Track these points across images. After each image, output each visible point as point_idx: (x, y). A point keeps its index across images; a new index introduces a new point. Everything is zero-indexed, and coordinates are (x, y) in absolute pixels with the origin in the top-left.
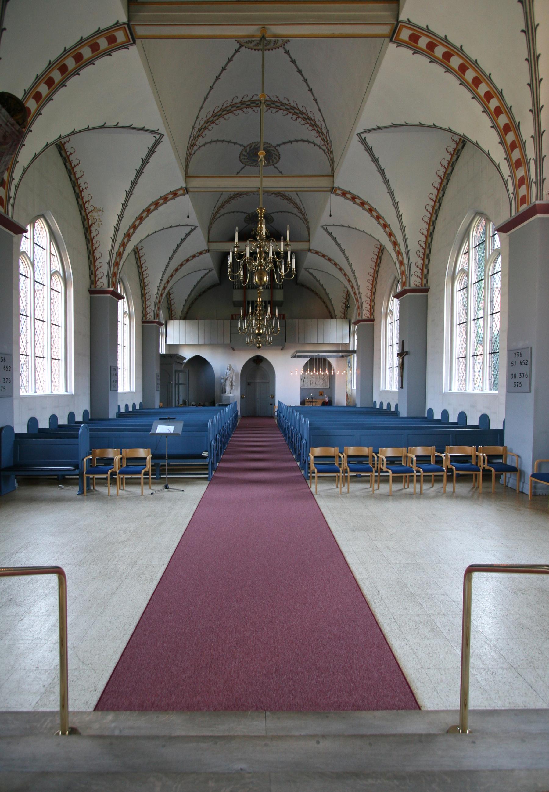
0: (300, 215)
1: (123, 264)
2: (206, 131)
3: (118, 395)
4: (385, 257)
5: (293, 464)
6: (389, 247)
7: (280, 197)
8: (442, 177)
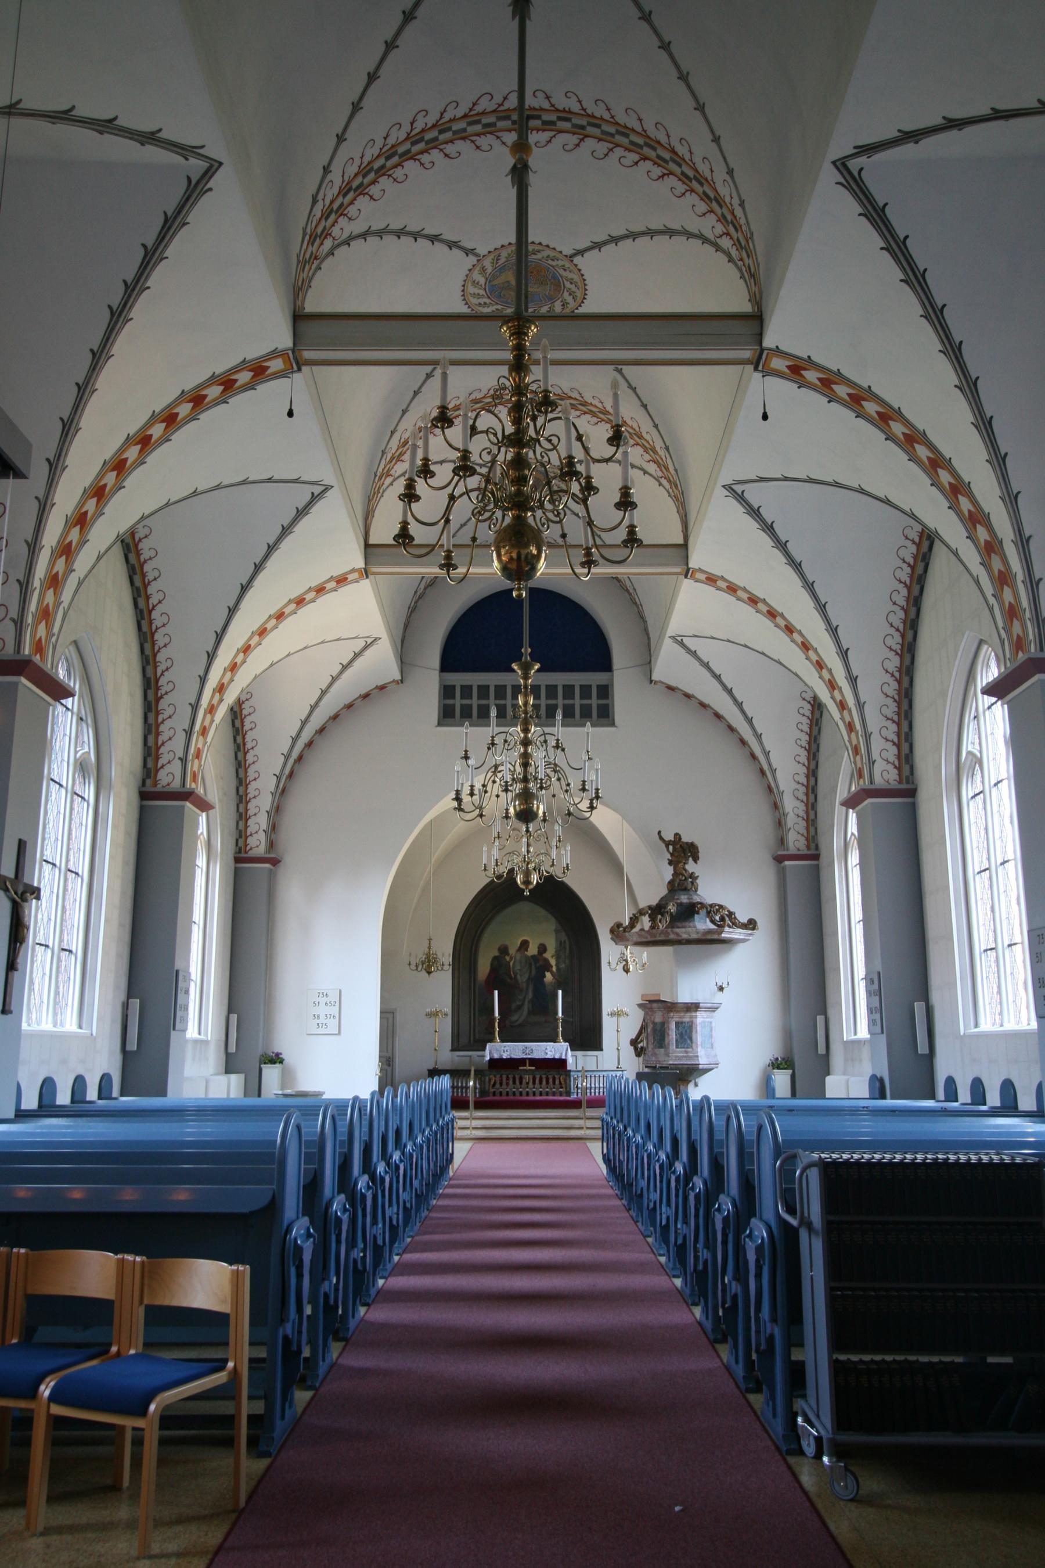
0: (652, 468)
1: (80, 584)
2: (362, 202)
3: (24, 1044)
4: (940, 559)
5: (660, 1281)
6: (824, 695)
7: (588, 417)
8: (908, 583)
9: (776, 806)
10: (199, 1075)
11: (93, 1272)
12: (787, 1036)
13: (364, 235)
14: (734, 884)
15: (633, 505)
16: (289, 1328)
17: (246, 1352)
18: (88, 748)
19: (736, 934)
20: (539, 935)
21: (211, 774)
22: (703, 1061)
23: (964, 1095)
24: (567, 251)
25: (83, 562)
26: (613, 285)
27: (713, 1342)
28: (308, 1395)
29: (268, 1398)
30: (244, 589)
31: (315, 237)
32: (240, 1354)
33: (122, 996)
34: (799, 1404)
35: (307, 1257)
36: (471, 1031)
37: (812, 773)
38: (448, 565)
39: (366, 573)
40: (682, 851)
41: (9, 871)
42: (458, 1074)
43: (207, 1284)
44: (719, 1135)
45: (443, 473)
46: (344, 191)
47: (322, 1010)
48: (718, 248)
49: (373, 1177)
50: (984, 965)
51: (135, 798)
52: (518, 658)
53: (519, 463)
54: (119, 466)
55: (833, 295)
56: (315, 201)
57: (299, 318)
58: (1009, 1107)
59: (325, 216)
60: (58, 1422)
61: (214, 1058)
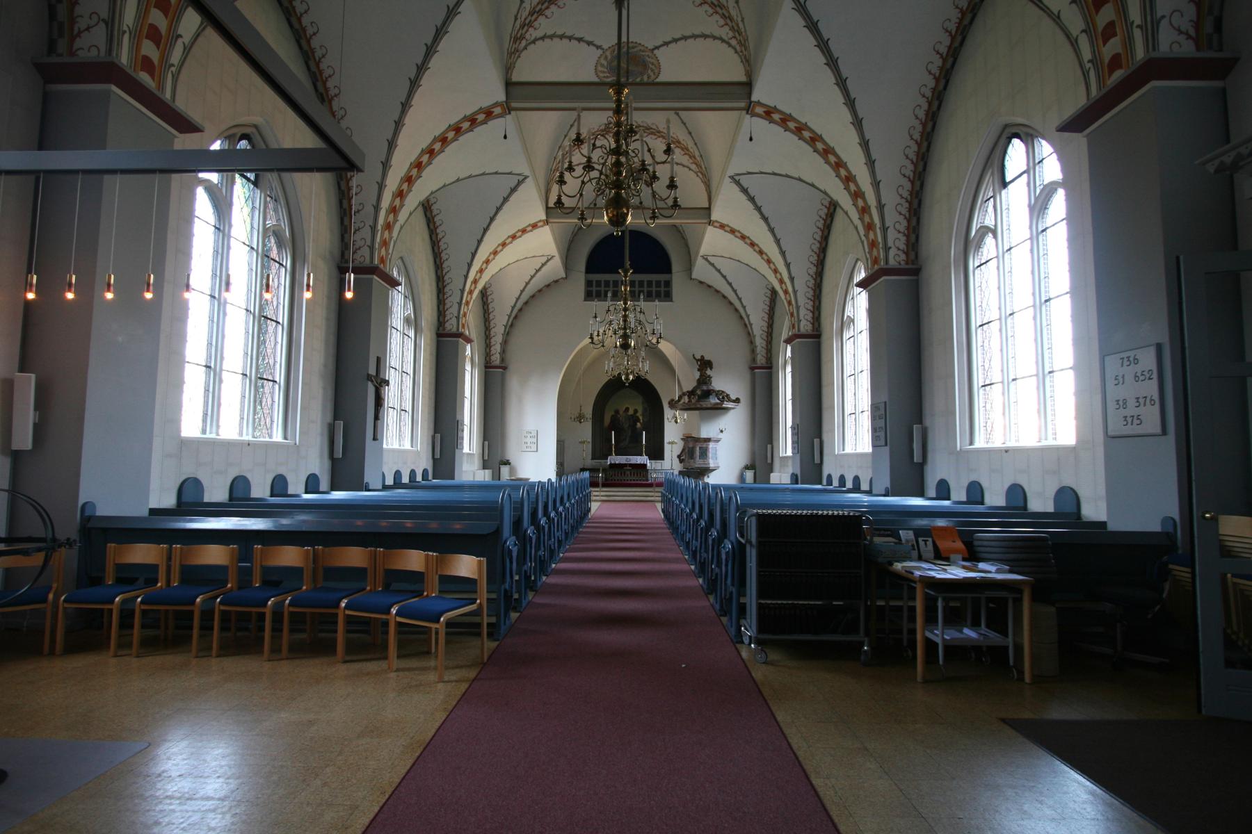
0: (693, 167)
2: (542, 19)
3: (385, 455)
5: (685, 567)
6: (844, 200)
9: (751, 343)
10: (470, 470)
11: (414, 560)
12: (753, 454)
13: (543, 38)
14: (729, 382)
15: (676, 187)
16: (507, 586)
17: (485, 596)
18: (410, 311)
19: (730, 405)
20: (634, 405)
21: (471, 323)
22: (712, 465)
23: (836, 483)
24: (651, 47)
25: (403, 216)
26: (676, 66)
27: (707, 594)
28: (517, 615)
29: (498, 616)
30: (485, 230)
31: (517, 39)
32: (482, 597)
33: (432, 433)
34: (743, 622)
35: (515, 554)
36: (600, 450)
37: (770, 325)
38: (582, 218)
39: (547, 222)
40: (705, 365)
41: (372, 371)
42: (593, 470)
43: (466, 566)
44: (713, 501)
45: (579, 171)
46: (531, 14)
47: (528, 440)
48: (730, 45)
49: (549, 518)
50: (849, 421)
51: (434, 336)
52: (622, 266)
53: (618, 164)
54: (419, 165)
55: (789, 72)
56: (516, 19)
57: (509, 85)
58: (856, 488)
59: (522, 27)
60: (400, 624)
61: (477, 462)
